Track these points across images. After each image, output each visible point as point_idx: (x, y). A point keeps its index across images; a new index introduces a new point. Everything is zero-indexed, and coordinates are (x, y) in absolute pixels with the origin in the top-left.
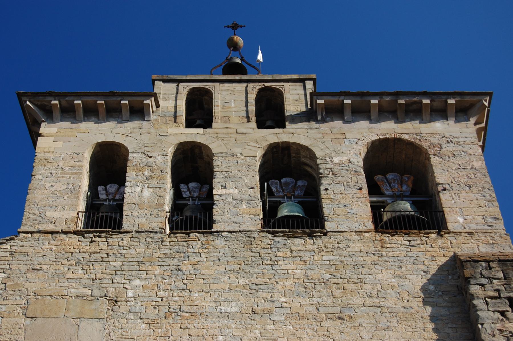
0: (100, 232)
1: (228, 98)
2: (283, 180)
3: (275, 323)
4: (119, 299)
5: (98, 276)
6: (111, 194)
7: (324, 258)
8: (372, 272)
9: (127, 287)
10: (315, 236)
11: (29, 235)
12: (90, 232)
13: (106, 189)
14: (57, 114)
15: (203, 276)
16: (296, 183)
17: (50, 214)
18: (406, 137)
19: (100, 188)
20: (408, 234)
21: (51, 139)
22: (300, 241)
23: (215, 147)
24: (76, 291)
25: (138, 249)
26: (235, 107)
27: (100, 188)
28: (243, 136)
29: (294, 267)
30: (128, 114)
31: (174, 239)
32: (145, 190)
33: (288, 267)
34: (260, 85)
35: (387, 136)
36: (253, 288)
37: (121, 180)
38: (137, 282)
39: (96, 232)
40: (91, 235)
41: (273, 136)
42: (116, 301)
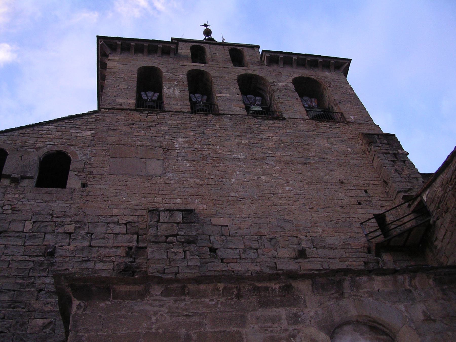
0: (153, 111)
1: (215, 52)
2: (248, 96)
3: (268, 165)
4: (169, 148)
5: (155, 134)
6: (149, 96)
7: (288, 131)
8: (316, 140)
9: (174, 141)
10: (279, 120)
11: (108, 110)
12: (146, 110)
13: (146, 94)
14: (119, 50)
15: (220, 138)
16: (255, 98)
17: (119, 100)
18: (313, 77)
19: (142, 93)
20: (328, 122)
21: (116, 63)
22: (271, 122)
23: (212, 73)
24: (142, 143)
25: (176, 121)
26: (219, 56)
27: (142, 93)
28: (227, 69)
29: (272, 135)
30: (161, 53)
31: (198, 117)
32: (176, 91)
33: (269, 135)
34: (231, 47)
35: (304, 76)
36: (250, 146)
37: (158, 88)
38: (181, 139)
39: (150, 110)
40: (147, 112)
41: (242, 71)
42: (168, 150)
